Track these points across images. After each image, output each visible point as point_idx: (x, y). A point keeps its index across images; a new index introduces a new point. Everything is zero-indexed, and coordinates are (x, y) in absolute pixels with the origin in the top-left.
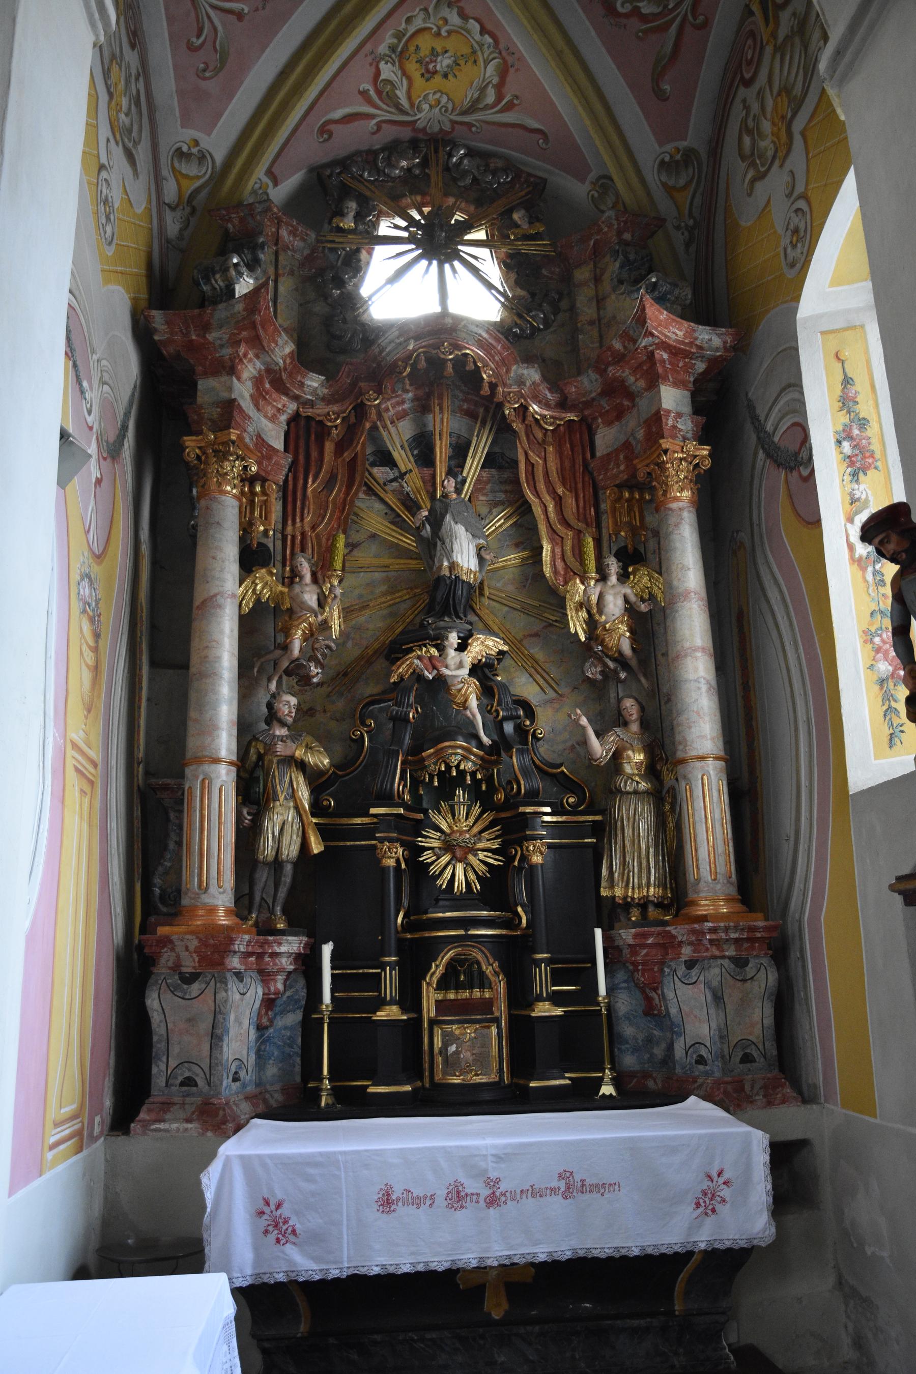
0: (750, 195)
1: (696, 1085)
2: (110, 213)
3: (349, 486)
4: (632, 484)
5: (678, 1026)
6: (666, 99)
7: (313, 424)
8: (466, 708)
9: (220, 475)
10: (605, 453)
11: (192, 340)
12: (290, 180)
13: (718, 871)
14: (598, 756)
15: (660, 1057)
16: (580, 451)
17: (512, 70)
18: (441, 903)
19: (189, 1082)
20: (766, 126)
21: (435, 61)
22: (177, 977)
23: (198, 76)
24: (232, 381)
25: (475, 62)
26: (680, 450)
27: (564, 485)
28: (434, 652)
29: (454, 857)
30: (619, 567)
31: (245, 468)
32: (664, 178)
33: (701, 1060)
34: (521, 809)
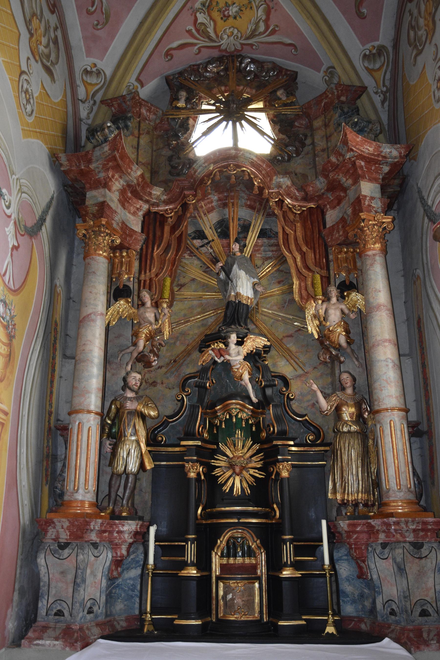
0: (414, 65)
1: (390, 630)
2: (30, 98)
3: (178, 251)
4: (346, 243)
5: (378, 587)
6: (365, 17)
7: (158, 216)
8: (242, 380)
9: (96, 245)
10: (331, 225)
11: (82, 170)
12: (151, 83)
13: (401, 483)
14: (325, 409)
15: (369, 608)
16: (317, 225)
17: (273, 11)
18: (225, 501)
19: (59, 613)
20: (422, 21)
21: (228, 10)
22: (56, 545)
23: (94, 28)
24: (105, 191)
25: (251, 8)
26: (373, 219)
27: (307, 245)
28: (222, 345)
29: (234, 472)
30: (338, 292)
31: (113, 241)
32: (366, 64)
33: (393, 613)
34: (275, 443)
